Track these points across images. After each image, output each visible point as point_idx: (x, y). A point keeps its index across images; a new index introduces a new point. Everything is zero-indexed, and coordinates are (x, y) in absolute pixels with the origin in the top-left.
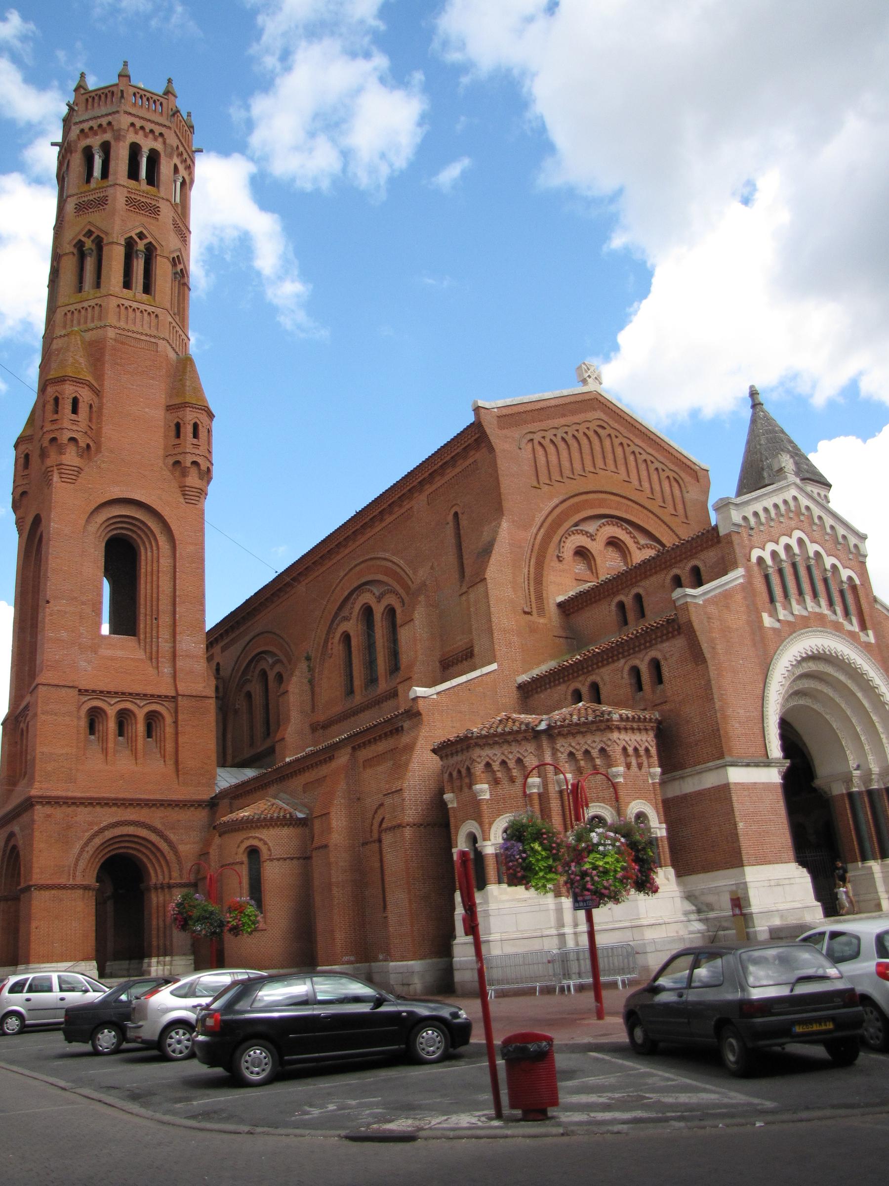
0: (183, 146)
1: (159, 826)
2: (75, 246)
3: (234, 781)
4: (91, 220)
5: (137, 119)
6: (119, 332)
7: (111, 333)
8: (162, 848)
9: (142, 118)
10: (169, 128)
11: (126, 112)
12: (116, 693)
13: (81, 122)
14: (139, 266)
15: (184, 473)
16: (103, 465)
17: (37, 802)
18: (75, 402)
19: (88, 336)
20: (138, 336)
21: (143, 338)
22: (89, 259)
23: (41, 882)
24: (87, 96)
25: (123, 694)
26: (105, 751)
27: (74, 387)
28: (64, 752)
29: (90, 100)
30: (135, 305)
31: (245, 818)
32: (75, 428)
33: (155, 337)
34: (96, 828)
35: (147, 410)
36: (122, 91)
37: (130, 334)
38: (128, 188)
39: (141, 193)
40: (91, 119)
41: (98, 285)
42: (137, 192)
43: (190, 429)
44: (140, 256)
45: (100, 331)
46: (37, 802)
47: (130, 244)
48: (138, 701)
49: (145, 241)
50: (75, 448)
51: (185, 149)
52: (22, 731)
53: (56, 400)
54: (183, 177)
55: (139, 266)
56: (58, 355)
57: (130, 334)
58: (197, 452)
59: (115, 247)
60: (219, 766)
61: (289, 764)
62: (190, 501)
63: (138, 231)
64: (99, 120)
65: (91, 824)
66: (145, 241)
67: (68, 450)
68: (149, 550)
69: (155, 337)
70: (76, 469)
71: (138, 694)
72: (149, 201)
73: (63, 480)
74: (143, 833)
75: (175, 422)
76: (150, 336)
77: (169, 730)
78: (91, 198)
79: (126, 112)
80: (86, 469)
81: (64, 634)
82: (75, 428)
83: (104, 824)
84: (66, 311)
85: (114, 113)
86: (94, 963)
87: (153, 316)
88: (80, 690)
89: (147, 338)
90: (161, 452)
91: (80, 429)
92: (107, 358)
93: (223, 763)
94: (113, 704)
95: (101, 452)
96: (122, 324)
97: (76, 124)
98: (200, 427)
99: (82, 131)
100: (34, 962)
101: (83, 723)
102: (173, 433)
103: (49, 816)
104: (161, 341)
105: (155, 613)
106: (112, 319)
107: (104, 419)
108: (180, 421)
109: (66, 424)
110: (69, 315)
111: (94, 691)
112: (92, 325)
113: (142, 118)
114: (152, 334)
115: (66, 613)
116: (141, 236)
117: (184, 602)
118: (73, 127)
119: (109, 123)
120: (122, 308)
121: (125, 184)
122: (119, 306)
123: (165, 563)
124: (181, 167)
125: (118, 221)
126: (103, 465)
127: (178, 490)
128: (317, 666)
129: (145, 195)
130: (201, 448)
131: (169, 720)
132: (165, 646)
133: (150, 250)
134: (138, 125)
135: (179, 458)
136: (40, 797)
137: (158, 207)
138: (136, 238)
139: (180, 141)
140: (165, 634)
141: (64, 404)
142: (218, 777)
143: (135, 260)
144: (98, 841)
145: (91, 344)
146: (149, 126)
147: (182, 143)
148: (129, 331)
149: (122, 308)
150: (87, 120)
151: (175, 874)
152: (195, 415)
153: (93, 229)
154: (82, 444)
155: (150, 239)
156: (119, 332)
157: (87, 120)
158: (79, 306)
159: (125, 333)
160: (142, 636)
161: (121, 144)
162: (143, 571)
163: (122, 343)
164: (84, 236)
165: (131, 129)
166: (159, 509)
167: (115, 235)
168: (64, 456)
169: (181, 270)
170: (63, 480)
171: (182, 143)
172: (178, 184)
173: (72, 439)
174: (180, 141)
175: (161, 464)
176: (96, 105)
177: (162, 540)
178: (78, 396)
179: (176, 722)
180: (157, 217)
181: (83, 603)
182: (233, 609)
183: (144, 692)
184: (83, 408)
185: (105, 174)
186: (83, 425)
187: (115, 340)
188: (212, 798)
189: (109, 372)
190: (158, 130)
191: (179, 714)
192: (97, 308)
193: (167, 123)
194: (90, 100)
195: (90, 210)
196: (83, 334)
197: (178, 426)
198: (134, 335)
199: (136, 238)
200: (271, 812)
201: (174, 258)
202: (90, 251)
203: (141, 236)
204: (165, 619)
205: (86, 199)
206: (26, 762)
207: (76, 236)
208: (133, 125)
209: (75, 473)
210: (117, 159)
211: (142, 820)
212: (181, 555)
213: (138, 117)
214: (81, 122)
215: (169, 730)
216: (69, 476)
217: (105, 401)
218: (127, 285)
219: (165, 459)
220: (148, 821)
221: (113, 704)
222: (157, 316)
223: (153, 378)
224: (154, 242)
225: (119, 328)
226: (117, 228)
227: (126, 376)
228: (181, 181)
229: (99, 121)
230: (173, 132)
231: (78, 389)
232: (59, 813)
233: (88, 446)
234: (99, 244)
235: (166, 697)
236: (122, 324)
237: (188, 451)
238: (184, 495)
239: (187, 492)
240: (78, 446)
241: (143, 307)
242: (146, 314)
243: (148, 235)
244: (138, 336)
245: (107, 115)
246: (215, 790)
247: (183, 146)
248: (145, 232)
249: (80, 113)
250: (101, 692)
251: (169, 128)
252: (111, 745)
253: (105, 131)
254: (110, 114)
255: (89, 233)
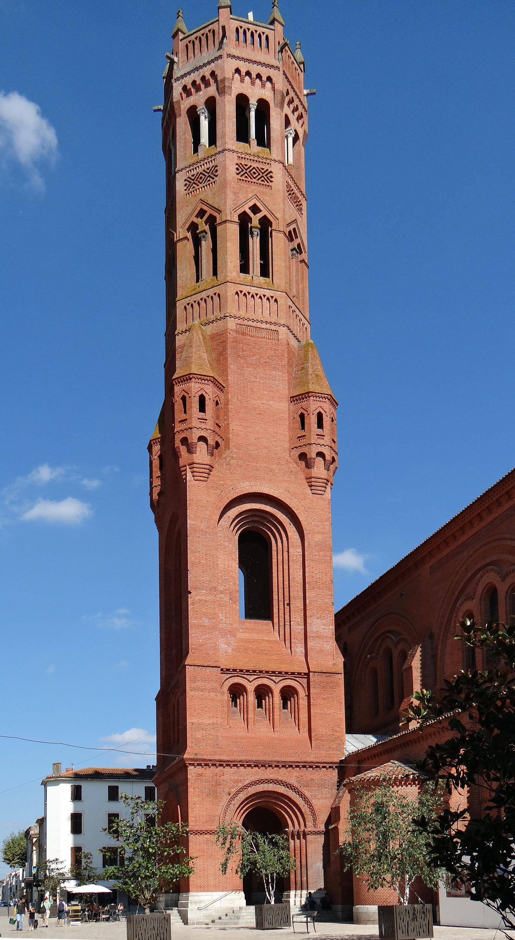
0: (294, 91)
1: (296, 784)
2: (188, 230)
3: (360, 746)
4: (202, 196)
5: (242, 62)
6: (239, 322)
7: (231, 324)
8: (298, 802)
9: (247, 60)
10: (278, 68)
11: (229, 56)
12: (254, 671)
13: (182, 77)
14: (255, 244)
15: (309, 465)
16: (232, 462)
17: (190, 764)
18: (202, 400)
19: (209, 330)
20: (259, 325)
21: (264, 326)
22: (203, 243)
23: (197, 828)
24: (186, 41)
25: (261, 672)
26: (247, 721)
27: (199, 385)
28: (211, 722)
29: (190, 46)
30: (253, 290)
31: (372, 778)
32: (203, 426)
33: (275, 324)
34: (240, 785)
35: (271, 403)
36: (224, 28)
37: (250, 323)
38: (237, 152)
39: (252, 158)
40: (193, 71)
41: (215, 273)
42: (247, 157)
43: (314, 419)
44: (255, 233)
45: (221, 323)
46: (190, 764)
47: (244, 219)
48: (274, 678)
49: (260, 215)
50: (205, 446)
51: (296, 94)
52: (174, 705)
53: (184, 399)
54: (295, 131)
55: (255, 244)
56: (181, 352)
57: (250, 323)
58: (322, 442)
59: (229, 225)
60: (347, 732)
61: (414, 731)
62: (316, 492)
63: (251, 204)
64: (201, 71)
65: (237, 781)
66: (260, 215)
67: (198, 449)
68: (279, 541)
69: (275, 324)
70: (208, 467)
71: (274, 672)
72: (260, 166)
73: (196, 478)
74: (282, 789)
75: (299, 413)
76: (271, 323)
77: (303, 702)
78: (200, 170)
79: (229, 56)
80: (216, 466)
81: (206, 621)
82: (203, 426)
83: (247, 782)
84: (185, 304)
85: (217, 59)
86: (242, 894)
87: (272, 301)
88: (222, 670)
89: (268, 326)
90: (287, 446)
91: (208, 428)
92: (229, 351)
93: (351, 729)
94: (252, 681)
95: (229, 448)
96: (241, 313)
97: (178, 79)
98: (324, 416)
99: (185, 88)
100: (193, 891)
101: (226, 697)
102: (298, 425)
103: (201, 775)
104: (281, 328)
105: (287, 599)
106: (231, 309)
107: (230, 414)
108: (304, 412)
109: (195, 423)
110: (189, 308)
111: (234, 670)
112: (212, 317)
113: (247, 60)
114: (273, 321)
115: (206, 601)
116: (255, 209)
117: (314, 588)
118: (175, 85)
119: (213, 74)
120: (241, 295)
121: (234, 148)
122: (237, 293)
123: (296, 551)
124: (293, 118)
125: (230, 195)
126: (232, 462)
127: (305, 482)
128: (440, 643)
129: (256, 159)
130: (325, 438)
131: (302, 693)
132: (298, 628)
133: (265, 223)
134: (243, 71)
135: (304, 450)
136: (192, 760)
137: (271, 172)
138: (249, 212)
139: (290, 84)
140: (297, 617)
141: (191, 402)
142: (346, 742)
143: (250, 239)
144: (242, 796)
145: (213, 337)
146: (255, 69)
147: (292, 88)
148: (249, 320)
149: (241, 295)
150: (189, 73)
151: (310, 824)
152: (319, 404)
153: (205, 208)
154: (211, 442)
155: (264, 213)
156: (239, 322)
157: (189, 73)
158: (197, 297)
159: (246, 322)
160: (276, 620)
161: (227, 97)
162: (274, 561)
163: (243, 334)
164: (197, 216)
165: (237, 75)
166: (287, 501)
167: (228, 212)
168: (195, 455)
169: (299, 245)
170: (196, 478)
171: (292, 88)
172: (290, 140)
173: (202, 439)
174: (290, 84)
175: (287, 457)
176: (197, 51)
177: (291, 529)
178: (204, 393)
179: (309, 696)
180: (270, 184)
181: (221, 592)
182: (358, 593)
183: (279, 670)
184: (209, 405)
185: (213, 140)
186: (210, 424)
187: (236, 331)
188: (341, 761)
189: (232, 367)
190: (265, 72)
191: (311, 689)
192: (216, 298)
193: (275, 63)
194: (190, 46)
195: (201, 185)
196: (203, 327)
197: (302, 416)
198: (254, 324)
199: (249, 212)
200: (397, 773)
201: (290, 232)
202: (204, 234)
203: (255, 209)
204: (297, 604)
205: (195, 172)
206: (179, 731)
207: (189, 218)
208: (238, 71)
209: (207, 471)
210: (224, 118)
211: (280, 778)
212: (309, 544)
213: (243, 59)
214: (182, 77)
215: (303, 702)
216: (202, 474)
217: (230, 397)
218: (244, 268)
219: (290, 452)
220: (284, 779)
221: (252, 681)
222: (276, 301)
223: (275, 369)
224: (269, 216)
225: (239, 318)
226: (230, 204)
227: (249, 369)
228: (293, 135)
229: (202, 72)
230: (281, 72)
231: (203, 386)
232: (209, 772)
233: (217, 443)
234: (212, 221)
235: (299, 674)
236: (241, 313)
237: (312, 442)
238: (310, 486)
239: (313, 483)
240: (207, 444)
241: (261, 292)
242: (264, 300)
243: (262, 208)
244: (259, 325)
245: (209, 63)
246: (344, 753)
247: (294, 91)
248: (259, 205)
249: (180, 65)
250: (241, 671)
251: (278, 68)
252: (251, 715)
253: (207, 84)
254: (212, 61)
255: (201, 214)
